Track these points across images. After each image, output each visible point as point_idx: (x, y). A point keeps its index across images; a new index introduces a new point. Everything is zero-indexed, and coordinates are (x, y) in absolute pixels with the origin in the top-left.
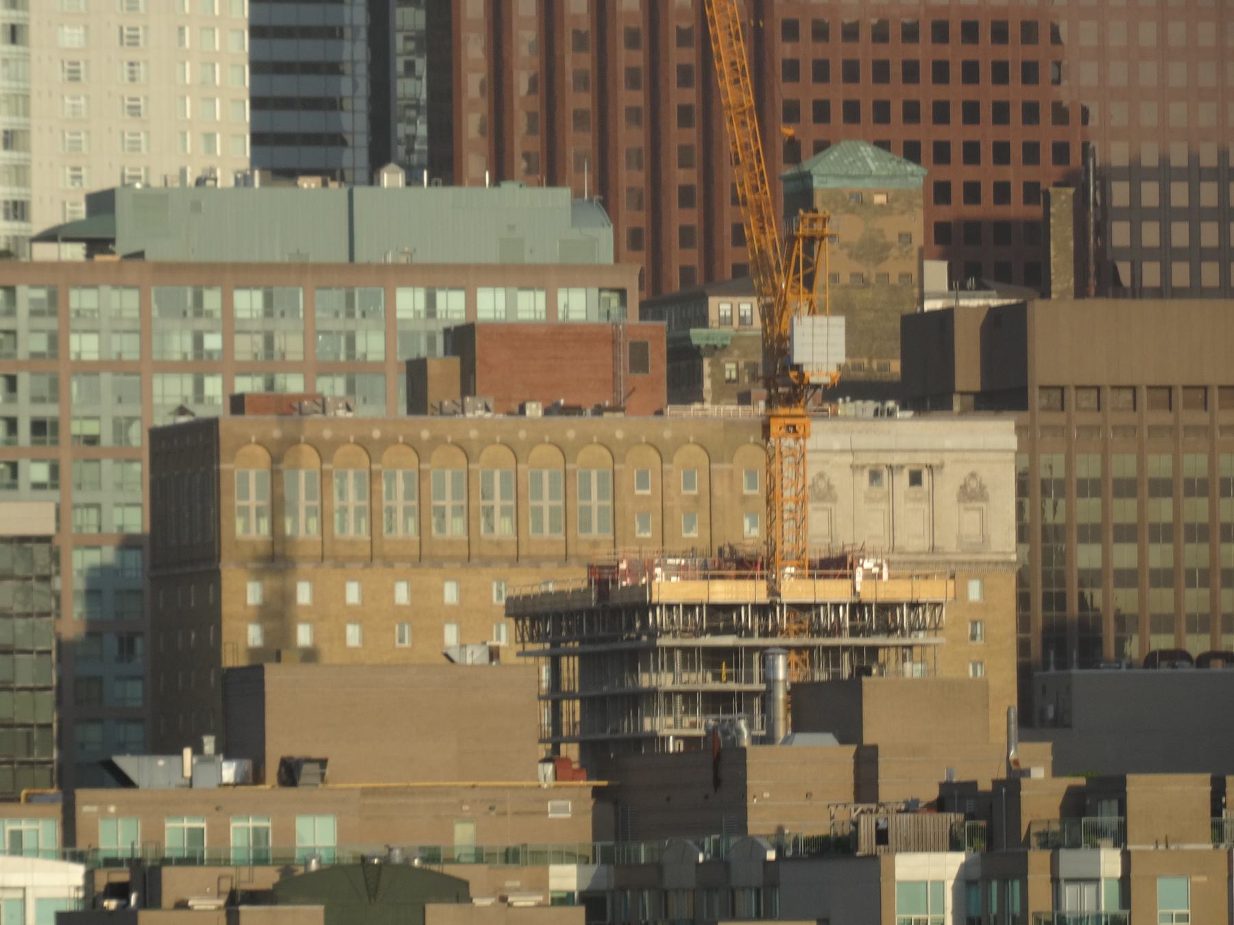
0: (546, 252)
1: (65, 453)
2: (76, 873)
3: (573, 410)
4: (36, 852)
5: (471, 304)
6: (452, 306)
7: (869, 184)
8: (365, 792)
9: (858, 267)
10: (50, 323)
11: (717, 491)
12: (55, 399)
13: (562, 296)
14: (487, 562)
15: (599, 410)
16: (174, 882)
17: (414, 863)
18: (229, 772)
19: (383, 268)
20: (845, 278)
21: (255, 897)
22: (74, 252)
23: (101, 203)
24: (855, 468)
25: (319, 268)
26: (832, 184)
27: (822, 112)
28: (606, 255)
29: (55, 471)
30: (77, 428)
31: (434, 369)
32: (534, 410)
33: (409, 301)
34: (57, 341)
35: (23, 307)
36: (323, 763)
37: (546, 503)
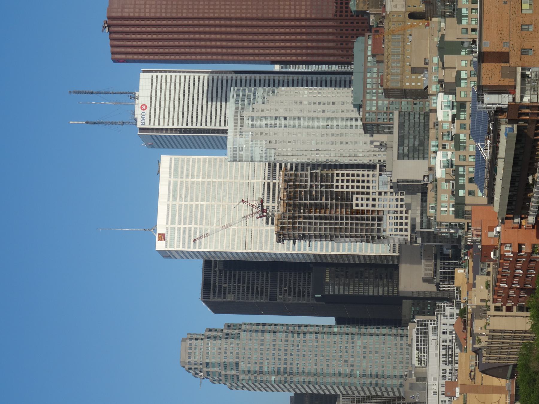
1: (388, 111)
2: (440, 94)
3: (384, 41)
4: (437, 99)
5: (369, 56)
6: (370, 59)
7: (355, 3)
8: (429, 52)
10: (371, 113)
11: (395, 20)
12: (381, 113)
15: (384, 37)
16: (441, 77)
18: (426, 72)
19: (365, 68)
21: (443, 65)
22: (361, 109)
23: (355, 106)
26: (355, 8)
27: (347, 12)
28: (363, 38)
29: (391, 113)
30: (385, 110)
31: (377, 59)
32: (383, 46)
33: (369, 65)
34: (373, 112)
35: (369, 117)
36: (425, 59)
37: (396, 44)
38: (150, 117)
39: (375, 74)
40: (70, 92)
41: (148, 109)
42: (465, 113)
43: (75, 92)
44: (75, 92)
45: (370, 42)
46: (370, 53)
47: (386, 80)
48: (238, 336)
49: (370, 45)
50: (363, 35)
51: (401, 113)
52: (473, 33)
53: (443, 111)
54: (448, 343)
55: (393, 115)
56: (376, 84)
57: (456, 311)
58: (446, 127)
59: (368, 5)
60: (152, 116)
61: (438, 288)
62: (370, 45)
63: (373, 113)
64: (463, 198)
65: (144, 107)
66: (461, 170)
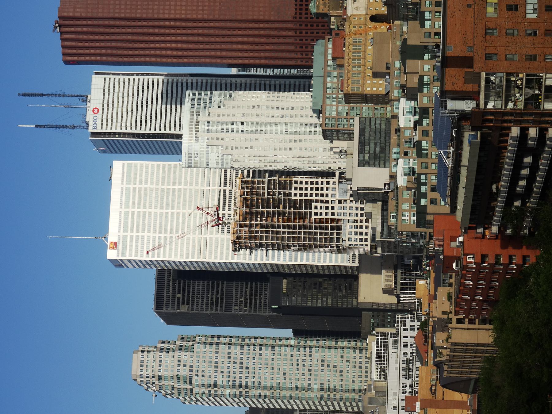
0: (323, 49)
1: (349, 117)
2: (402, 99)
3: (344, 44)
6: (330, 62)
8: (391, 57)
9: (327, 6)
13: (329, 47)
14: (365, 56)
15: (344, 40)
16: (403, 82)
17: (520, 182)
20: (328, 8)
22: (321, 115)
23: (314, 111)
24: (354, 4)
25: (324, 81)
26: (315, 10)
28: (323, 41)
29: (351, 119)
30: (345, 115)
31: (338, 63)
32: (344, 49)
35: (328, 122)
36: (387, 63)
38: (102, 120)
39: (335, 78)
40: (19, 95)
41: (100, 112)
42: (428, 120)
43: (24, 95)
44: (24, 95)
45: (330, 45)
46: (330, 57)
47: (346, 85)
48: (192, 349)
49: (330, 48)
50: (323, 38)
51: (362, 119)
52: (437, 37)
53: (405, 117)
54: (408, 357)
55: (353, 121)
56: (336, 77)
57: (417, 324)
58: (408, 133)
59: (328, 7)
60: (105, 120)
61: (399, 300)
62: (330, 48)
63: (333, 118)
64: (425, 207)
65: (96, 111)
66: (423, 177)
